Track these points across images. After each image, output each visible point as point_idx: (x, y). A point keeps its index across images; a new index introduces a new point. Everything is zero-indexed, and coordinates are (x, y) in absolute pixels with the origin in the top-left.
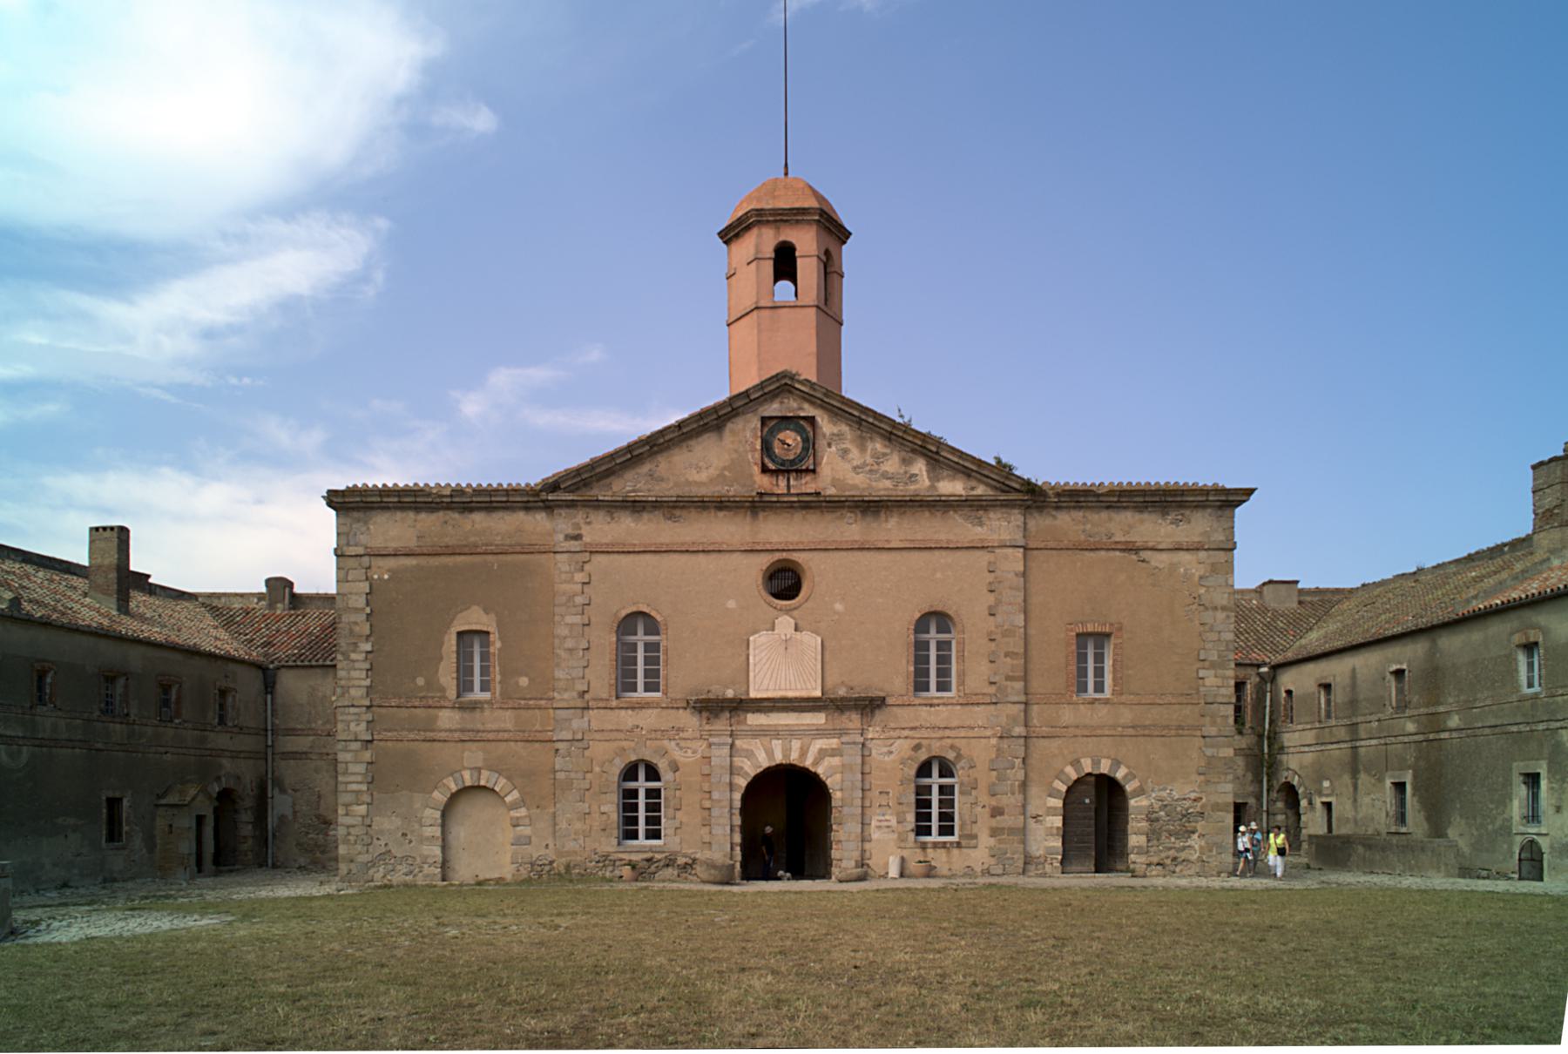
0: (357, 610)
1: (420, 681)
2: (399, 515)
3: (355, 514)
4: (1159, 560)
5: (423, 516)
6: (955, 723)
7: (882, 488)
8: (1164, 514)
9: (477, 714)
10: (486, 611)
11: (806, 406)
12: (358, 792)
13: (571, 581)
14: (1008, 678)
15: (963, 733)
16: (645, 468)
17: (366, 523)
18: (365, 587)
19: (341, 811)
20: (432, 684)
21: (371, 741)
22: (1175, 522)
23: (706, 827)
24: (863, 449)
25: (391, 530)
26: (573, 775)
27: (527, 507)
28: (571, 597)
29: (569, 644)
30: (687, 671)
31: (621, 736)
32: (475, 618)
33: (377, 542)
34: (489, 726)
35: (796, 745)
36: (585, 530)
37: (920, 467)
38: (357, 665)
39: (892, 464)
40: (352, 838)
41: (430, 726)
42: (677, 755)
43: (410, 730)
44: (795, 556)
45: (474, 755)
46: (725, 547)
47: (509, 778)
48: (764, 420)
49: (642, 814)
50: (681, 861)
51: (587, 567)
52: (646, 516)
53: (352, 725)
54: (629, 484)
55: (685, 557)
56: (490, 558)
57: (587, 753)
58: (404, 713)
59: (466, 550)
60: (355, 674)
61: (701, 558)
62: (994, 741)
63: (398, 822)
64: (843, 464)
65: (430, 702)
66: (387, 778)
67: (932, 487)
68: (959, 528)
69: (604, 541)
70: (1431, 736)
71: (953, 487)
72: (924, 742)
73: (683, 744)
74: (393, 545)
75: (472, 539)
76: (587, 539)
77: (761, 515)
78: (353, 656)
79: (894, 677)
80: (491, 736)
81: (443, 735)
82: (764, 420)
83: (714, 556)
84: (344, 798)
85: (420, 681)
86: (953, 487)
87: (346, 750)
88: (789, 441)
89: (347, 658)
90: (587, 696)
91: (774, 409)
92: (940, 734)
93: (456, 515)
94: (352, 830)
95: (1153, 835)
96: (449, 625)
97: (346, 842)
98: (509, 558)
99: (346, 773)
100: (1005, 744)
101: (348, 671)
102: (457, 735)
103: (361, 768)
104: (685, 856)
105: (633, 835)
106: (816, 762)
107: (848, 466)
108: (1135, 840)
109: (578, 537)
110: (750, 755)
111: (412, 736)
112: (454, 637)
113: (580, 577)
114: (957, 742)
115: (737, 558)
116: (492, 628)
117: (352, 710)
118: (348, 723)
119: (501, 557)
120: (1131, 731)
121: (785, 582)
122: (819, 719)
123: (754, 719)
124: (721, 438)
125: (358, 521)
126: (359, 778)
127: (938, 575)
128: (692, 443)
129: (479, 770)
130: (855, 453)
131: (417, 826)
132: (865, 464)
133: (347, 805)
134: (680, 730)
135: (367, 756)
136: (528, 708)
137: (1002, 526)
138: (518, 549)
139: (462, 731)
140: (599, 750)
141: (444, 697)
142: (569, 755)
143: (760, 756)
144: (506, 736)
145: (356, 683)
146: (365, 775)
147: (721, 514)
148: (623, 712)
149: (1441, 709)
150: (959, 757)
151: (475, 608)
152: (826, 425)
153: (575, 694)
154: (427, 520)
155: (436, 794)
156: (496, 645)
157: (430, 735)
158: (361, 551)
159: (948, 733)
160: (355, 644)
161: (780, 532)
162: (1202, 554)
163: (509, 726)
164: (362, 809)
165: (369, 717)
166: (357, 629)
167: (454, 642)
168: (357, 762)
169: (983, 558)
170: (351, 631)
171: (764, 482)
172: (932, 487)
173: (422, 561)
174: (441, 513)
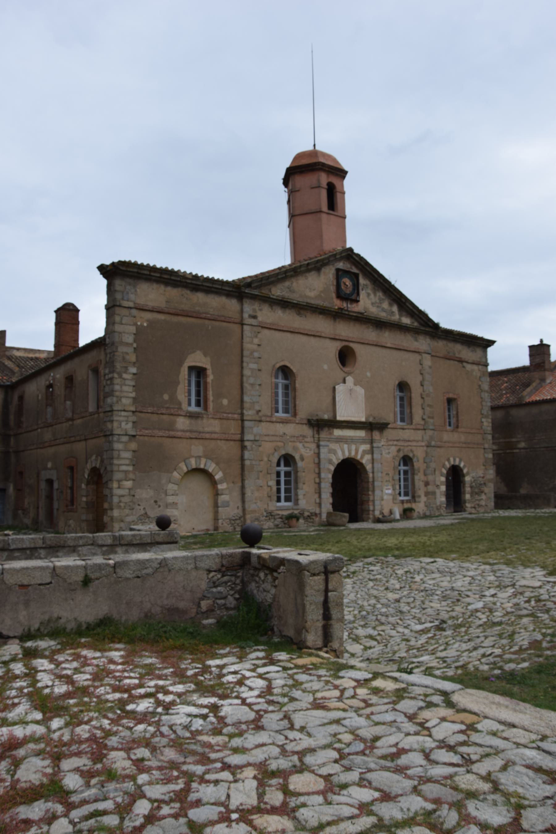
0: (128, 344)
1: (166, 397)
2: (155, 286)
3: (128, 280)
4: (469, 367)
5: (169, 289)
6: (412, 439)
7: (383, 315)
8: (469, 347)
9: (199, 421)
10: (205, 355)
11: (353, 267)
12: (126, 472)
13: (251, 343)
14: (429, 417)
15: (415, 444)
16: (287, 284)
17: (135, 287)
18: (133, 329)
19: (115, 485)
20: (173, 398)
21: (134, 436)
22: (472, 351)
23: (316, 496)
24: (375, 295)
25: (151, 294)
26: (254, 463)
27: (229, 295)
28: (252, 353)
29: (252, 380)
30: (309, 403)
31: (278, 439)
32: (197, 359)
33: (141, 301)
34: (206, 429)
35: (353, 447)
36: (259, 314)
37: (395, 308)
38: (128, 382)
39: (385, 305)
40: (122, 505)
41: (171, 427)
42: (303, 451)
43: (160, 429)
44: (352, 345)
45: (197, 449)
46: (323, 335)
47: (217, 464)
48: (338, 270)
49: (283, 487)
50: (306, 514)
51: (259, 335)
52: (288, 311)
53: (123, 424)
54: (277, 291)
55: (304, 338)
56: (207, 322)
57: (261, 449)
58: (155, 417)
59: (194, 315)
60: (125, 388)
61: (312, 339)
62: (425, 448)
63: (151, 493)
64: (369, 302)
65: (172, 411)
66: (152, 462)
67: (400, 319)
68: (407, 341)
69: (268, 321)
70: (508, 451)
71: (406, 321)
72: (402, 448)
73: (306, 445)
74: (151, 304)
75: (197, 308)
76: (260, 319)
77: (338, 320)
78: (125, 376)
79: (389, 411)
80: (207, 436)
81: (179, 434)
82: (338, 270)
83: (318, 339)
84: (117, 476)
85: (166, 397)
86: (406, 321)
87: (119, 441)
88: (347, 284)
89: (121, 377)
90: (260, 414)
91: (341, 265)
92: (406, 444)
93: (188, 292)
94: (123, 499)
95: (472, 494)
96: (181, 364)
97: (119, 507)
98: (217, 323)
99: (119, 458)
100: (429, 449)
101: (121, 386)
102: (188, 434)
103: (128, 455)
104: (308, 511)
105: (279, 500)
106: (362, 457)
107: (370, 302)
108: (468, 496)
109: (255, 317)
110: (334, 452)
111: (161, 434)
112: (186, 369)
113: (256, 341)
114: (414, 448)
115: (328, 341)
116: (208, 366)
117: (123, 413)
118: (120, 422)
119: (213, 322)
120: (464, 445)
121: (345, 356)
122: (361, 434)
123: (338, 432)
124: (319, 275)
125: (130, 285)
126: (127, 462)
127: (404, 363)
128: (307, 275)
129: (200, 457)
130: (372, 296)
131: (163, 495)
132: (376, 303)
133: (119, 481)
134: (304, 437)
135: (133, 446)
136: (228, 419)
137: (423, 343)
138: (223, 319)
139: (191, 431)
140: (267, 447)
141: (180, 408)
142: (252, 450)
143: (341, 453)
144: (216, 436)
145: (125, 394)
146: (131, 460)
147: (321, 316)
148: (278, 425)
149: (514, 440)
150: (414, 455)
151: (198, 352)
152: (362, 281)
153: (254, 412)
154: (173, 293)
155: (175, 474)
156: (210, 378)
157: (172, 433)
158: (131, 304)
159: (410, 443)
160: (126, 368)
161: (345, 330)
162: (480, 367)
163: (217, 429)
164: (129, 484)
165: (134, 418)
166: (127, 357)
167: (186, 373)
168: (126, 450)
169: (417, 357)
170: (124, 359)
171: (338, 304)
172: (400, 319)
173: (162, 317)
174: (180, 289)
